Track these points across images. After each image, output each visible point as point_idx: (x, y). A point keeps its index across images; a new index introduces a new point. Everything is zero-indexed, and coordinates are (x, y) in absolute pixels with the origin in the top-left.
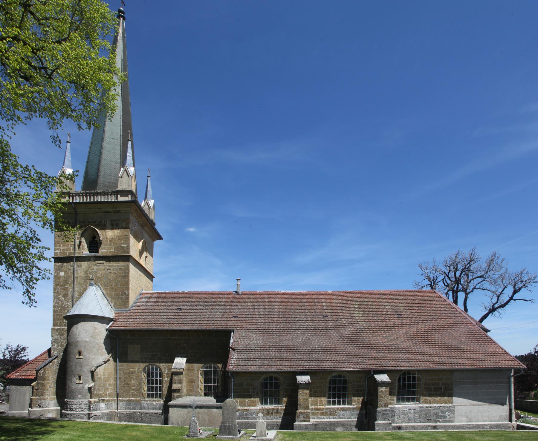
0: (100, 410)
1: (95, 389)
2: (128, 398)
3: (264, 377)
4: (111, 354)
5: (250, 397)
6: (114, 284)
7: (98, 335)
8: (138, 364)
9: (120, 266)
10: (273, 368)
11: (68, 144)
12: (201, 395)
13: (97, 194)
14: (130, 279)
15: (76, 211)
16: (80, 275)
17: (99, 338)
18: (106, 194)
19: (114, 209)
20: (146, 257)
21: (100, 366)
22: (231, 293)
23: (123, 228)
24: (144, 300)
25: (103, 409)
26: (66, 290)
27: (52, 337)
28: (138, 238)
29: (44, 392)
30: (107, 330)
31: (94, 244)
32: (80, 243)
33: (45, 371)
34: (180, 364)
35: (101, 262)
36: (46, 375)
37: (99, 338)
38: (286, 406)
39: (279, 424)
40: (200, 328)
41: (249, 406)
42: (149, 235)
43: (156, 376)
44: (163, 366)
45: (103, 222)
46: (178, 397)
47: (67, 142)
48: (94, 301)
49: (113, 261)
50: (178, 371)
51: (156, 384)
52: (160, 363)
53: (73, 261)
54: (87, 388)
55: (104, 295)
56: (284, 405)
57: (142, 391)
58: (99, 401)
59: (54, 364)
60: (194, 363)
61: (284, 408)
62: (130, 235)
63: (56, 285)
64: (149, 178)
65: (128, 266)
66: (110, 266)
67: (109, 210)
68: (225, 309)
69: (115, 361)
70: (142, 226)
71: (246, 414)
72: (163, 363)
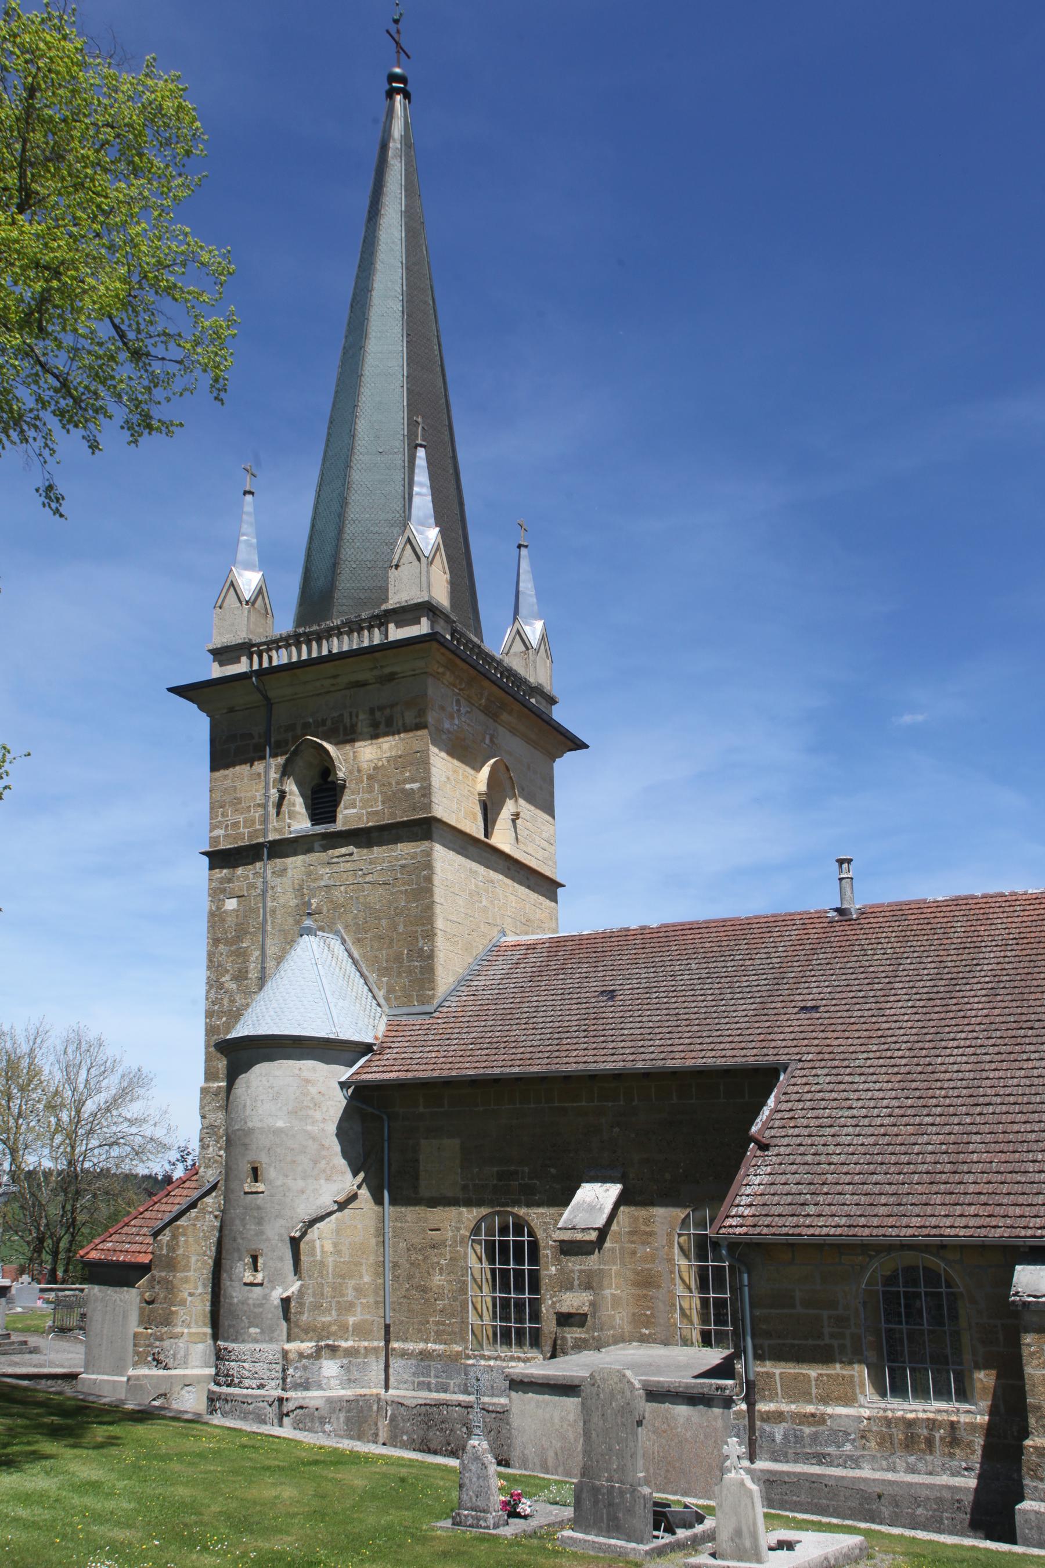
0: (320, 1387)
1: (301, 1304)
2: (421, 1346)
3: (879, 1267)
4: (361, 1176)
5: (824, 1356)
6: (384, 922)
7: (317, 1105)
8: (452, 1212)
9: (403, 857)
10: (910, 1226)
11: (249, 497)
12: (686, 1342)
13: (328, 634)
14: (437, 898)
15: (266, 698)
16: (281, 901)
17: (318, 1115)
18: (355, 627)
19: (376, 673)
20: (516, 816)
21: (321, 1219)
22: (820, 915)
23: (406, 730)
24: (499, 968)
25: (334, 1382)
26: (242, 955)
27: (203, 1117)
28: (465, 752)
29: (172, 1313)
30: (343, 1085)
31: (324, 796)
32: (282, 795)
33: (174, 1237)
34: (592, 1208)
35: (343, 850)
36: (180, 1252)
37: (318, 1115)
38: (993, 1412)
39: (968, 1499)
40: (660, 1064)
41: (825, 1400)
42: (528, 741)
43: (519, 1260)
44: (535, 1216)
45: (347, 720)
46: (580, 1346)
47: (246, 493)
48: (319, 989)
49: (380, 843)
50: (579, 1236)
51: (520, 1289)
52: (529, 1205)
53: (262, 860)
54: (277, 1302)
55: (355, 962)
56: (985, 1404)
57: (472, 1318)
58: (319, 1350)
59: (204, 1212)
60: (652, 1204)
61: (983, 1419)
62: (434, 750)
63: (215, 941)
64: (524, 552)
65: (429, 854)
66: (372, 862)
67: (360, 677)
68: (778, 981)
69: (379, 1201)
70: (492, 712)
71: (815, 1438)
72: (539, 1205)
